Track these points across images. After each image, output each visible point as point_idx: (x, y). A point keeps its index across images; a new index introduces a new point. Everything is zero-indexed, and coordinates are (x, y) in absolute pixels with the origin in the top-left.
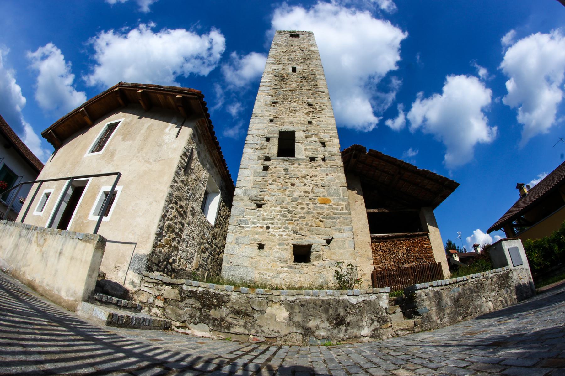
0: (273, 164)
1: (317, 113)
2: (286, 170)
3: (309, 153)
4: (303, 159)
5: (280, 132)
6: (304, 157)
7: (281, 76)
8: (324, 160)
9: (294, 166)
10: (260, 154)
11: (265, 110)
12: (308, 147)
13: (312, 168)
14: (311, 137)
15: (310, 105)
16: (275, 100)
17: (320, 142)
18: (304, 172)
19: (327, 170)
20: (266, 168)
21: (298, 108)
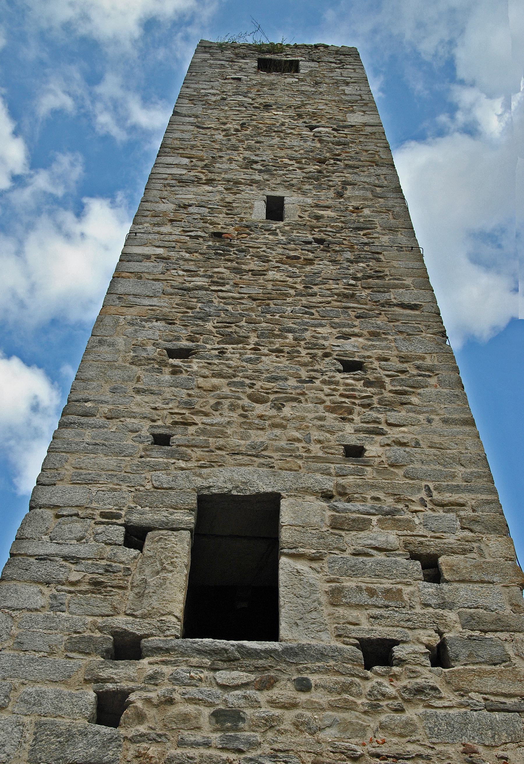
0: (153, 678)
1: (387, 405)
2: (227, 718)
3: (354, 614)
4: (322, 655)
5: (201, 499)
6: (327, 640)
7: (217, 235)
8: (439, 656)
9: (275, 693)
10: (84, 617)
11: (130, 386)
12: (350, 583)
13: (374, 708)
14: (361, 525)
15: (350, 366)
16: (184, 343)
17: (414, 556)
18: (328, 735)
19: (466, 721)
20: (110, 709)
21: (292, 382)
